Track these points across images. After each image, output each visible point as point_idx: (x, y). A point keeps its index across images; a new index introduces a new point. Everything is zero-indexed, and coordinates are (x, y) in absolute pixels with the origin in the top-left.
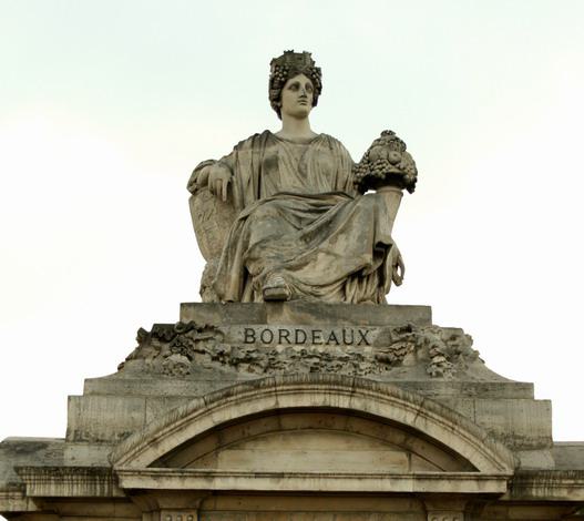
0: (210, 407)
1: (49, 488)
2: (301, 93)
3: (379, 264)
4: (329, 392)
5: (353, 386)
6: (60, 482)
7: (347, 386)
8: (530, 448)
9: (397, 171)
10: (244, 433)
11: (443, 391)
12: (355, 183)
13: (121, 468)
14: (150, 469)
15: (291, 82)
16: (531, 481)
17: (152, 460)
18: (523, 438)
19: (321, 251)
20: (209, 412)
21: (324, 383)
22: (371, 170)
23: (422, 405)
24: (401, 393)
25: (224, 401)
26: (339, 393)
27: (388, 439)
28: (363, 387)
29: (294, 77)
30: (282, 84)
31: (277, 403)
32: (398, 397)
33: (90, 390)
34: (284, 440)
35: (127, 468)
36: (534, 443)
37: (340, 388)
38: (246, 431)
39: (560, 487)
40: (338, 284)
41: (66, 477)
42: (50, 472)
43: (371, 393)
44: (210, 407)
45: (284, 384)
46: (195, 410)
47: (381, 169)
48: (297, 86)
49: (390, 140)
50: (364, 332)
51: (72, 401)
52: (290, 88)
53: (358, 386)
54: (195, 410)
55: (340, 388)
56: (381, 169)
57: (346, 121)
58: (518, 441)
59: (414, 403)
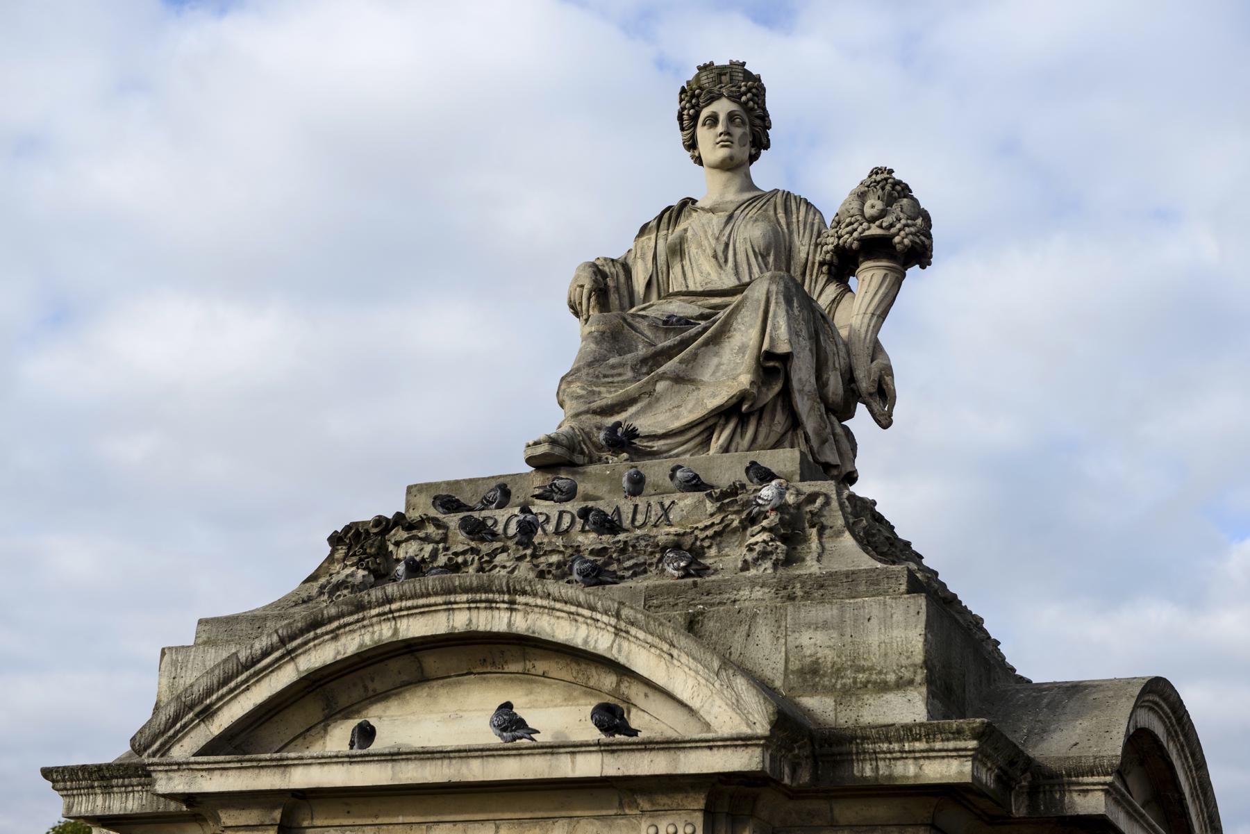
0: (290, 646)
1: (95, 801)
2: (720, 128)
3: (777, 388)
4: (473, 605)
5: (509, 592)
6: (107, 790)
7: (501, 592)
8: (883, 687)
9: (879, 232)
10: (366, 688)
11: (745, 593)
12: (822, 264)
13: (152, 760)
14: (200, 759)
15: (705, 113)
16: (845, 749)
17: (202, 743)
18: (871, 669)
19: (662, 377)
20: (291, 655)
21: (466, 590)
22: (839, 238)
23: (618, 616)
24: (582, 598)
25: (312, 634)
26: (490, 605)
27: (591, 683)
28: (524, 593)
29: (730, 107)
30: (694, 118)
31: (396, 631)
32: (579, 605)
33: (204, 637)
34: (429, 695)
35: (164, 760)
36: (891, 678)
37: (491, 596)
38: (371, 686)
39: (904, 755)
40: (696, 431)
41: (114, 782)
42: (90, 774)
43: (539, 602)
44: (290, 646)
45: (402, 598)
46: (265, 654)
47: (851, 233)
48: (713, 120)
49: (889, 188)
50: (667, 503)
51: (167, 658)
52: (704, 124)
53: (516, 592)
54: (265, 654)
55: (491, 596)
56: (851, 233)
57: (824, 174)
58: (862, 677)
59: (606, 612)
